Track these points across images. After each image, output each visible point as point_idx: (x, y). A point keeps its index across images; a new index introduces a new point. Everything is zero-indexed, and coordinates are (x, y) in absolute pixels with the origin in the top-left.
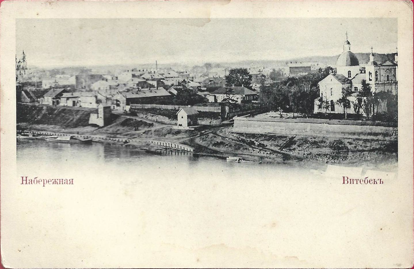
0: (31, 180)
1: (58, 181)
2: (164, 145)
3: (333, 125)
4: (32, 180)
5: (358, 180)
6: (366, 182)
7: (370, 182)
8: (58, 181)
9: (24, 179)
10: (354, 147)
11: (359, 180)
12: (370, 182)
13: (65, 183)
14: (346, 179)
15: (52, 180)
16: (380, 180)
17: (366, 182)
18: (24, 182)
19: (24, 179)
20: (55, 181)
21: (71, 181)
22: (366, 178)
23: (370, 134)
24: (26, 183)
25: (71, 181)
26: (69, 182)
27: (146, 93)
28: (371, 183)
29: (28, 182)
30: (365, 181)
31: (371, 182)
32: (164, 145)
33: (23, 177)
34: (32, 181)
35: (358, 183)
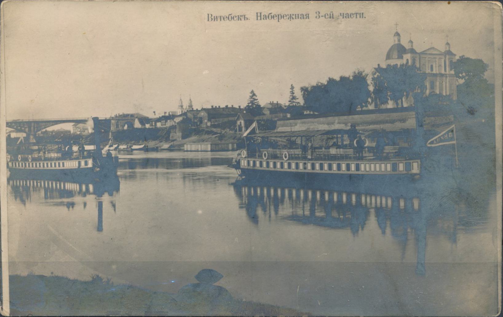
0: (265, 16)
1: (294, 17)
2: (372, 170)
3: (204, 152)
4: (266, 16)
5: (221, 17)
6: (230, 19)
7: (283, 18)
8: (294, 17)
9: (259, 15)
10: (324, 170)
11: (222, 16)
12: (283, 18)
13: (264, 19)
14: (210, 16)
15: (287, 15)
16: (245, 16)
17: (230, 19)
18: (259, 18)
19: (259, 15)
20: (291, 17)
21: (307, 15)
22: (270, 14)
23: (217, 169)
24: (261, 19)
25: (307, 15)
26: (305, 17)
27: (343, 19)
28: (235, 20)
29: (262, 17)
30: (231, 18)
31: (235, 18)
32: (372, 170)
33: (257, 13)
34: (266, 17)
35: (357, 17)
